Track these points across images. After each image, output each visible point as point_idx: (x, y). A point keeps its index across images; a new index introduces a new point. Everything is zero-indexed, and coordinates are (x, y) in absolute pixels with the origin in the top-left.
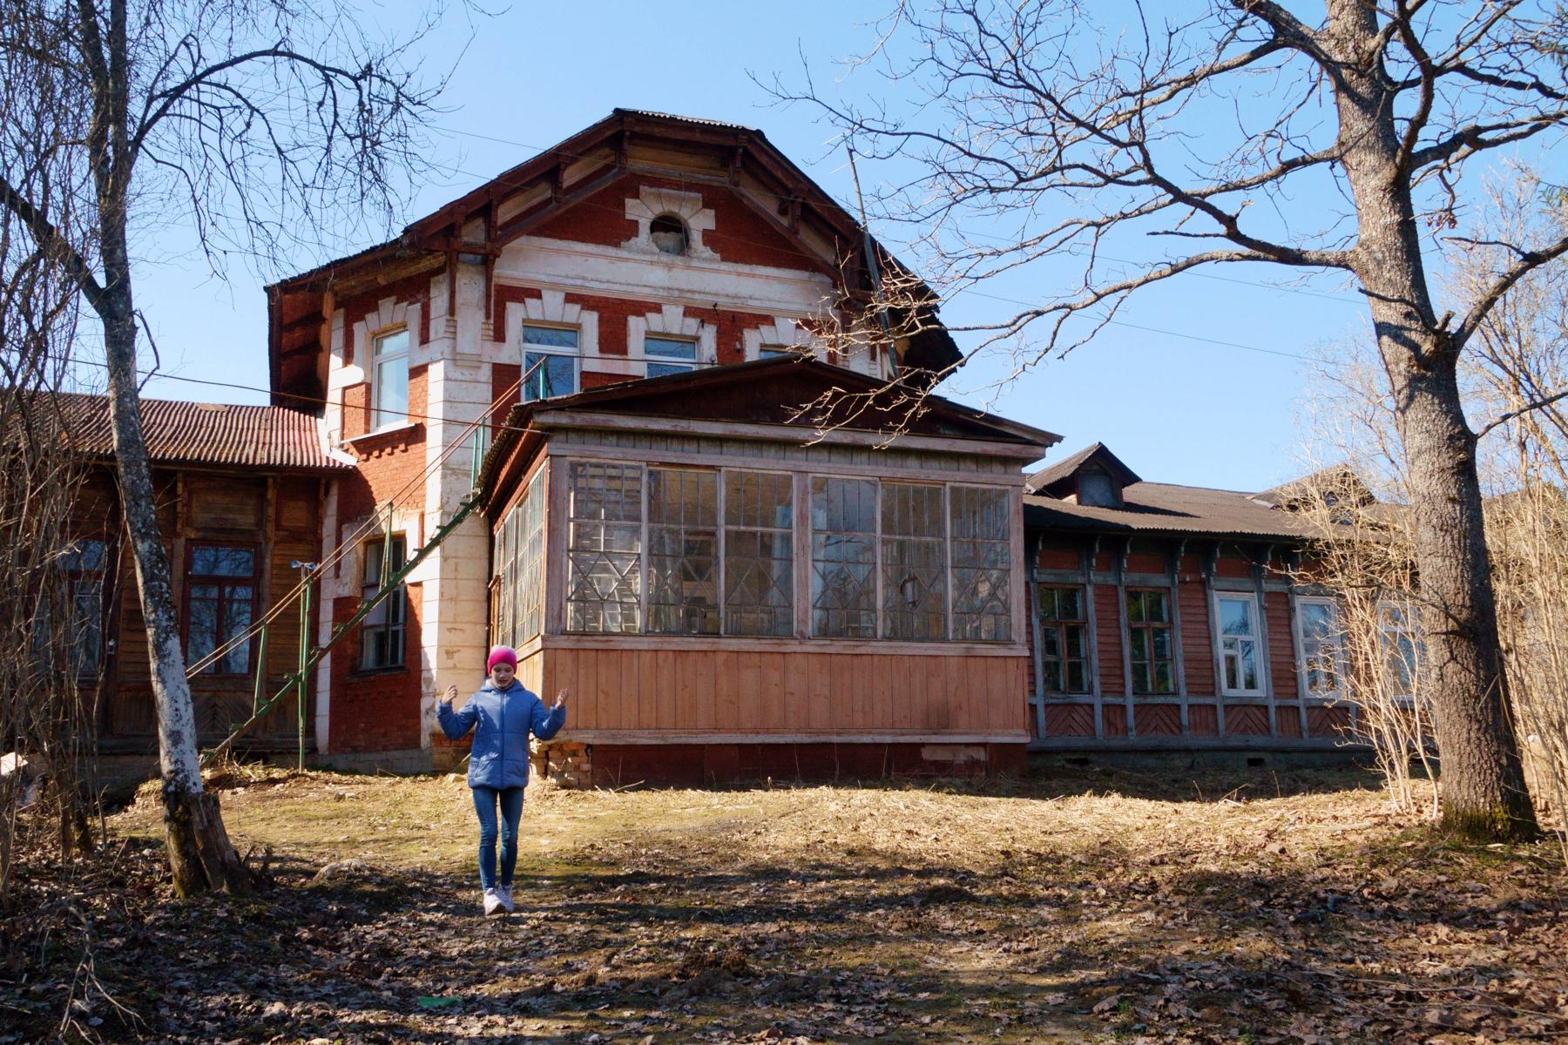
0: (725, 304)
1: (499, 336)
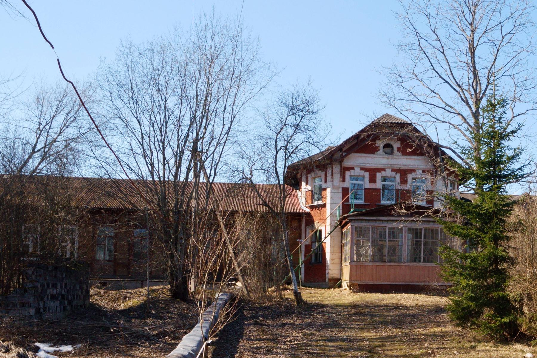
0: (402, 167)
1: (344, 180)
